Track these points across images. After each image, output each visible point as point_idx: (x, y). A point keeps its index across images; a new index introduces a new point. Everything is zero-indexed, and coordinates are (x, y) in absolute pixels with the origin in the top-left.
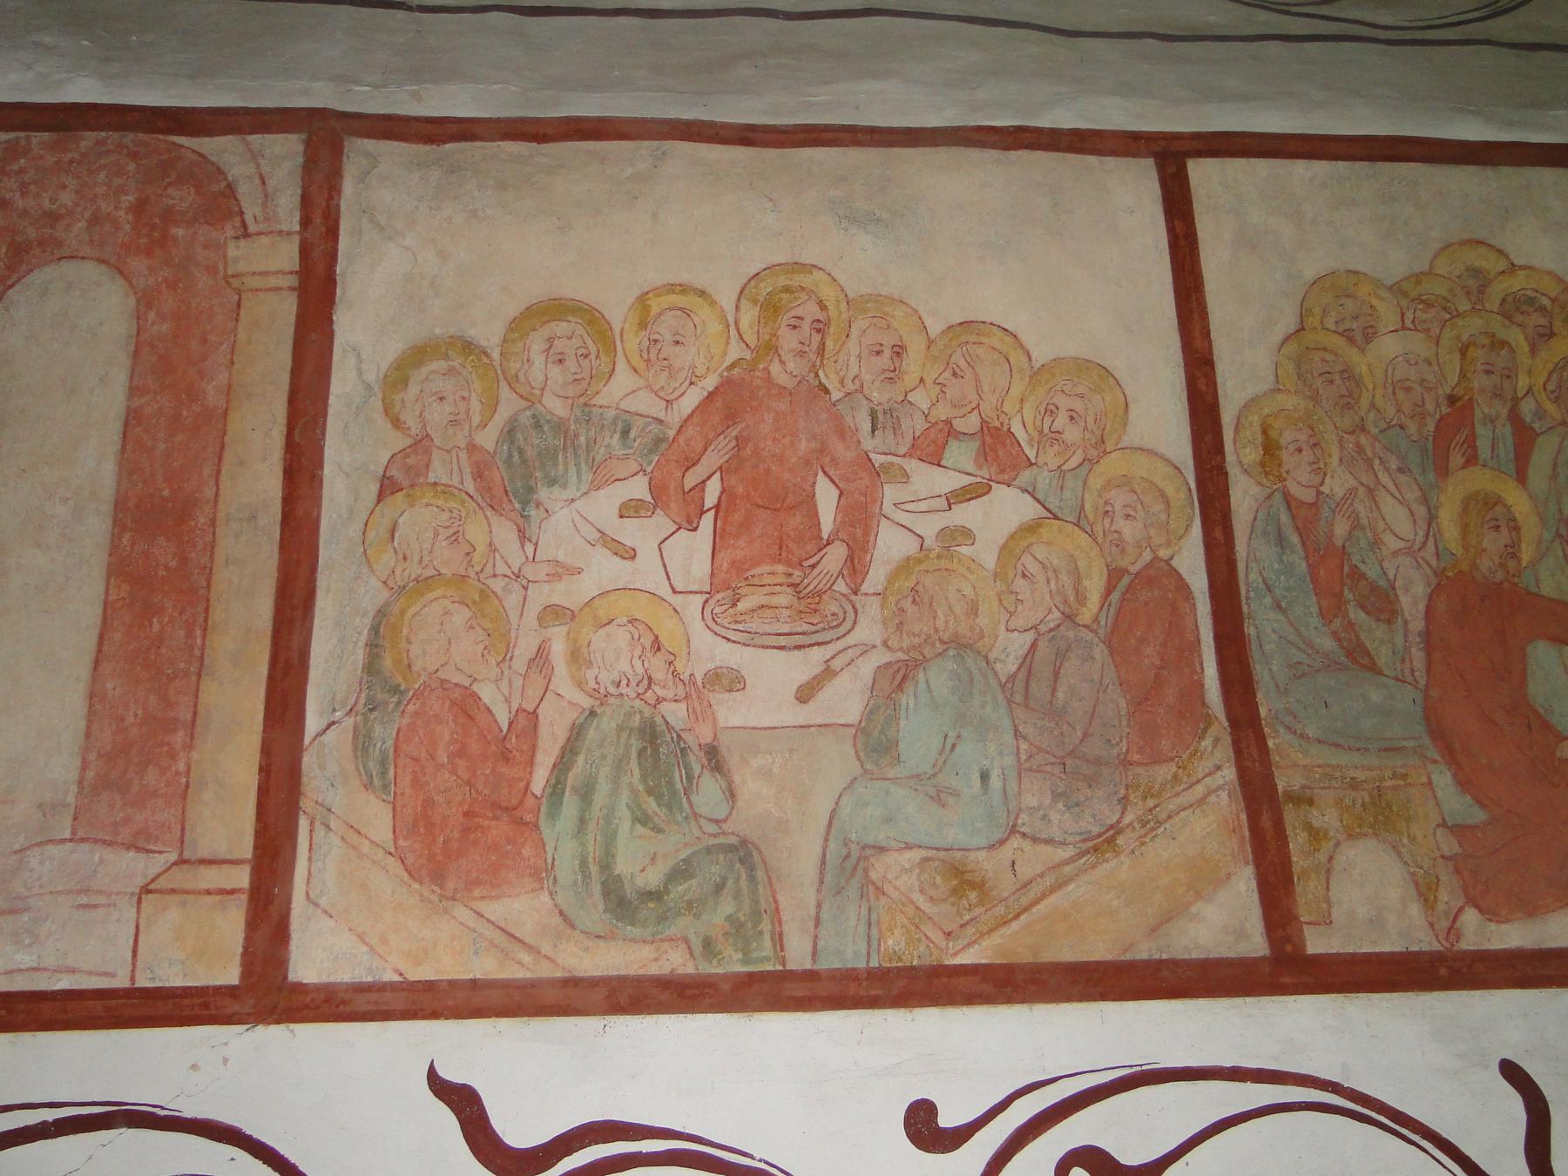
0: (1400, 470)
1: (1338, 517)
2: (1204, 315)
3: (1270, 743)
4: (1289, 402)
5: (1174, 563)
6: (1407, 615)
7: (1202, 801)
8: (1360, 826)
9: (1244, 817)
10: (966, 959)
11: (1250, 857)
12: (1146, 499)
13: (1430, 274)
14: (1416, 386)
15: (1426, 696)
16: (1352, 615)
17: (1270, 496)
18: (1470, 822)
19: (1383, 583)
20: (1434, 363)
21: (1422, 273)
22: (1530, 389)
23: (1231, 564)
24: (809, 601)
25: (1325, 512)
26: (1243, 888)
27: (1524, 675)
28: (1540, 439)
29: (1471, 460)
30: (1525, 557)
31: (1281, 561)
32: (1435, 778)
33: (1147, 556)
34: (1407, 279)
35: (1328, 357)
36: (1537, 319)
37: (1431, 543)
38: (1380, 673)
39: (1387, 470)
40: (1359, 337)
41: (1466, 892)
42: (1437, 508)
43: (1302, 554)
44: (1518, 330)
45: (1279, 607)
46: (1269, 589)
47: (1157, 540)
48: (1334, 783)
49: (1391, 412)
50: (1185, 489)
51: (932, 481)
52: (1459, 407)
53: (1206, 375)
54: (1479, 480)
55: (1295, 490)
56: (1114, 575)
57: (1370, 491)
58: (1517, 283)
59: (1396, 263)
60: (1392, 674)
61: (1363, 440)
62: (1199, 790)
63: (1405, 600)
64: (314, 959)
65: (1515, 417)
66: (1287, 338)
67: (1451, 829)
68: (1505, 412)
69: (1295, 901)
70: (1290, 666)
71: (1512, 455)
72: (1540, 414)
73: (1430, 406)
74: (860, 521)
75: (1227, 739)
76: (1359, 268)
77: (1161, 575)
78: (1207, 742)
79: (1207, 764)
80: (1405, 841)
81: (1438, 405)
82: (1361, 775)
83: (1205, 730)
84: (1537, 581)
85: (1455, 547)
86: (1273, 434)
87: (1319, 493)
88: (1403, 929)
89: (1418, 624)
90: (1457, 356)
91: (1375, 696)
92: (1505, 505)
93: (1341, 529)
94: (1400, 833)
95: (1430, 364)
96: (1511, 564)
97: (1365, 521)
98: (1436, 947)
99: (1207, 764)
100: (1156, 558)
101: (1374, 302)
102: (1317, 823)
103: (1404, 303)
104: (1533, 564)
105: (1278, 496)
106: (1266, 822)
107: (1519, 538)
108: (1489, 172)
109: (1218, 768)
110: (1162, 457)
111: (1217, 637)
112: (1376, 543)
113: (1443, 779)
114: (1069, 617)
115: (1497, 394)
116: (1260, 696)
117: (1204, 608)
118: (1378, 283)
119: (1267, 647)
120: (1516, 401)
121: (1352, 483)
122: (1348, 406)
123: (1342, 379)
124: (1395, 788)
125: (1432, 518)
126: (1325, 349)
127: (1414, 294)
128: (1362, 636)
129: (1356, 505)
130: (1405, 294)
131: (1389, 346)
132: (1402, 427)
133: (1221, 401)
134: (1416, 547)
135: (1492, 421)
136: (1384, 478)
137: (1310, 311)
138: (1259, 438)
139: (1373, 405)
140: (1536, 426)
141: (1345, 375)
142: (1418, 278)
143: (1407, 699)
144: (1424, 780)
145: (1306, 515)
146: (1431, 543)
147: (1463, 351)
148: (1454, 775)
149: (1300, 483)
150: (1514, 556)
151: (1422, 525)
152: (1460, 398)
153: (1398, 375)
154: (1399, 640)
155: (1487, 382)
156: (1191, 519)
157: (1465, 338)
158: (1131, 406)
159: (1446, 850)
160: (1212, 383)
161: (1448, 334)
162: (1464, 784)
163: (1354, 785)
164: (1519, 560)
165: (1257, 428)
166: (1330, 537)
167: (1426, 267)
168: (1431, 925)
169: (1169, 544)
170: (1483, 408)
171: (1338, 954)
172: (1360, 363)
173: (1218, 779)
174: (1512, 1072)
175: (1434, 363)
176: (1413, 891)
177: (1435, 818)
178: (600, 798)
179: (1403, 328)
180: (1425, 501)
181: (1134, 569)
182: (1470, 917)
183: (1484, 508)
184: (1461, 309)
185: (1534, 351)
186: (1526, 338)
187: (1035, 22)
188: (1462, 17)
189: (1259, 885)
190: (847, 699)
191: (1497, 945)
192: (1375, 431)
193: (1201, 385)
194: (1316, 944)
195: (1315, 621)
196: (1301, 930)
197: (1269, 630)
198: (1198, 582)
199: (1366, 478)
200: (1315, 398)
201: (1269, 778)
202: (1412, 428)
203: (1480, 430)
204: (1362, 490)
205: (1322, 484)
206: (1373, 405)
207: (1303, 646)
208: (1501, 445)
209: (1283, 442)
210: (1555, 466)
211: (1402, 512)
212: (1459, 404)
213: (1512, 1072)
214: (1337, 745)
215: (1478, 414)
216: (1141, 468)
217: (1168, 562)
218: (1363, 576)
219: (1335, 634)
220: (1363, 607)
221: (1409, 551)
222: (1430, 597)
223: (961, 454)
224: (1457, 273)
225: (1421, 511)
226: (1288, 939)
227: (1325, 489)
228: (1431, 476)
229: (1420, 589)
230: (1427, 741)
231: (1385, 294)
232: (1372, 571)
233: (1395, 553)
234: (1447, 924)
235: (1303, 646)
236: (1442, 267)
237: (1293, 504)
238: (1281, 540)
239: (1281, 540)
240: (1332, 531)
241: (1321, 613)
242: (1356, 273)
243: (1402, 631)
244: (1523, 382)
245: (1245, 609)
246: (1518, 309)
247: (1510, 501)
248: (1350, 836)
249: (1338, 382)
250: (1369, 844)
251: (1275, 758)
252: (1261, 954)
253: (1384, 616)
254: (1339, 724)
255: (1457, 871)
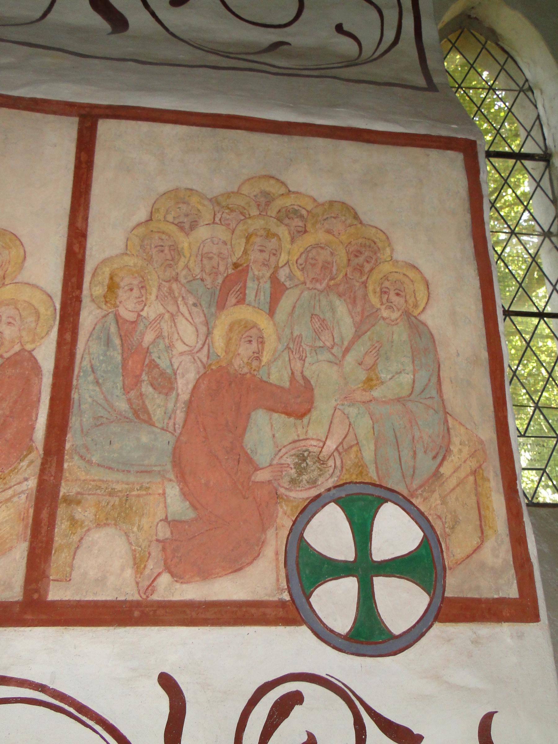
0: (195, 305)
1: (148, 330)
3: (66, 465)
4: (131, 261)
5: (34, 353)
6: (180, 391)
7: (8, 500)
8: (107, 519)
9: (31, 511)
11: (28, 537)
12: (24, 314)
13: (238, 193)
14: (215, 257)
15: (178, 440)
16: (143, 390)
17: (105, 316)
18: (183, 518)
19: (169, 371)
20: (229, 243)
21: (233, 193)
22: (288, 262)
23: (72, 355)
25: (141, 327)
26: (18, 556)
27: (245, 429)
28: (287, 292)
29: (241, 301)
30: (265, 360)
31: (105, 355)
32: (168, 491)
33: (17, 348)
34: (222, 195)
35: (164, 237)
36: (297, 222)
37: (206, 348)
38: (153, 425)
39: (186, 304)
40: (187, 226)
41: (165, 563)
42: (213, 328)
43: (120, 351)
44: (286, 228)
45: (97, 382)
46: (93, 371)
47: (26, 338)
48: (98, 491)
49: (198, 270)
50: (52, 309)
52: (240, 270)
53: (80, 243)
54: (244, 313)
55: (123, 312)
57: (172, 315)
58: (288, 202)
59: (218, 185)
60: (160, 426)
61: (174, 286)
62: (10, 492)
63: (180, 382)
65: (274, 279)
66: (139, 225)
67: (169, 523)
68: (268, 275)
69: (50, 565)
70: (94, 418)
71: (268, 300)
72: (291, 277)
73: (222, 269)
75: (39, 462)
76: (194, 187)
78: (24, 464)
79: (20, 477)
80: (135, 529)
81: (227, 268)
82: (118, 487)
83: (26, 456)
84: (269, 374)
85: (220, 352)
86: (117, 279)
87: (139, 315)
88: (119, 585)
89: (185, 396)
90: (244, 240)
91: (144, 439)
92: (259, 329)
93: (149, 337)
94: (133, 525)
95: (226, 244)
96: (255, 363)
97: (165, 334)
98: (137, 597)
99: (20, 477)
100: (23, 350)
101: (200, 207)
102: (77, 517)
103: (217, 208)
104: (269, 364)
105: (111, 316)
106: (45, 515)
107: (263, 349)
108: (286, 138)
109: (26, 479)
110: (41, 289)
111: (52, 399)
112: (170, 347)
113: (173, 491)
115: (265, 264)
116: (69, 436)
117: (47, 381)
118: (202, 196)
119: (83, 407)
120: (277, 268)
121: (162, 310)
122: (170, 266)
123: (170, 250)
124: (138, 496)
125: (209, 333)
126: (163, 233)
127: (224, 204)
128: (147, 402)
129: (162, 324)
130: (219, 204)
131: (202, 232)
132: (202, 280)
133: (87, 257)
134: (195, 350)
135: (258, 279)
136: (183, 309)
137: (158, 210)
138: (107, 281)
139: (187, 266)
140: (287, 284)
141: (172, 248)
142: (229, 195)
143: (164, 442)
144: (161, 491)
146: (206, 348)
147: (248, 238)
148: (181, 489)
149: (127, 309)
150: (258, 359)
151: (202, 338)
152: (241, 265)
153: (206, 250)
154: (171, 406)
155: (260, 257)
156: (52, 327)
157: (251, 230)
158: (27, 258)
159: (161, 536)
160: (83, 247)
161: (241, 227)
162: (185, 495)
163: (112, 493)
164: (261, 361)
165: (107, 275)
166: (140, 344)
167: (235, 190)
168: (137, 583)
169: (33, 341)
170: (255, 271)
171: (69, 601)
172: (184, 242)
173: (24, 486)
174: (167, 682)
175: (229, 243)
176: (131, 563)
177: (161, 515)
179: (214, 223)
180: (207, 324)
181: (6, 355)
182: (165, 579)
183: (246, 331)
184: (252, 214)
185: (293, 240)
186: (290, 233)
187: (65, 48)
188: (331, 66)
189: (29, 555)
191: (177, 597)
192: (183, 281)
193: (76, 248)
194: (56, 593)
195: (118, 392)
196: (48, 585)
197: (87, 396)
199: (172, 308)
200: (150, 260)
201: (57, 487)
202: (209, 280)
203: (250, 284)
204: (167, 316)
205: (143, 310)
206: (187, 266)
207: (106, 406)
208: (262, 294)
209: (122, 284)
210: (294, 307)
211: (190, 329)
212: (240, 268)
213: (167, 682)
214: (110, 468)
215: (250, 274)
216: (26, 294)
217: (30, 352)
218: (157, 366)
219: (129, 401)
220: (152, 385)
221: (190, 353)
222: (198, 380)
224: (255, 193)
225: (203, 330)
226: (37, 591)
227: (144, 314)
228: (213, 310)
229: (192, 376)
230: (169, 467)
231: (206, 202)
232: (163, 364)
233: (182, 354)
234: (148, 583)
235: (106, 406)
236: (245, 190)
237: (120, 321)
238: (108, 342)
239: (108, 342)
240: (143, 338)
241: (124, 387)
242: (191, 190)
243: (174, 400)
244: (283, 258)
245: (75, 382)
246: (287, 216)
247: (262, 326)
248: (98, 525)
249: (166, 251)
250: (111, 530)
251: (66, 474)
252: (16, 599)
253: (165, 391)
254: (116, 455)
255: (164, 549)
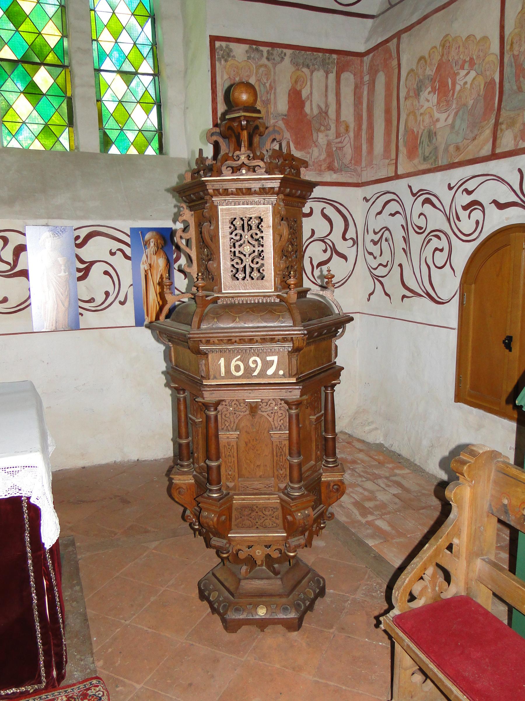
2: (504, 20)
10: (456, 161)
24: (447, 101)
51: (463, 73)
56: (485, 83)
64: (399, 173)
74: (454, 84)
77: (493, 80)
114: (479, 95)
145: (516, 58)
177: (522, 122)
178: (424, 143)
190: (450, 121)
198: (497, 80)
223: (466, 66)
238: (512, 66)
239: (512, 66)
